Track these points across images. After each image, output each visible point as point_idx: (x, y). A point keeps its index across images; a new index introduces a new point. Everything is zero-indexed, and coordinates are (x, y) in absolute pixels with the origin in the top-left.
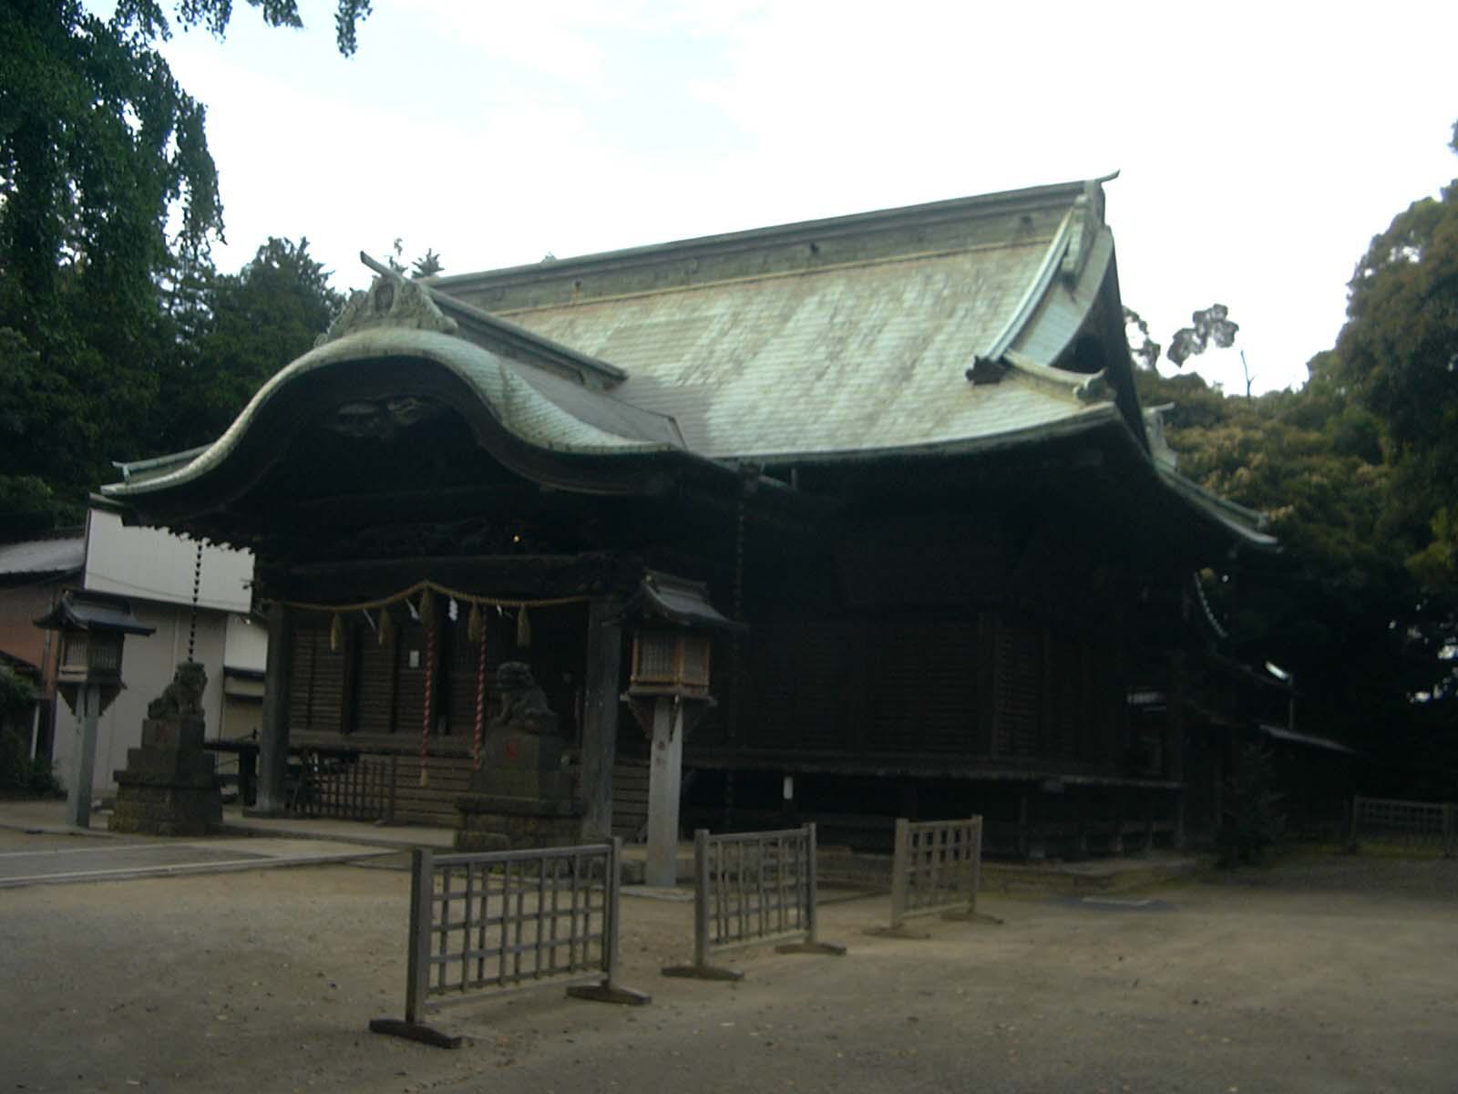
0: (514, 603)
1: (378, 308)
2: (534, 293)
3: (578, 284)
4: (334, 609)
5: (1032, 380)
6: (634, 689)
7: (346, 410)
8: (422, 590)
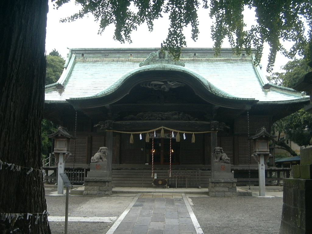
0: (182, 132)
1: (160, 57)
3: (131, 55)
6: (55, 151)
7: (152, 82)
8: (162, 128)
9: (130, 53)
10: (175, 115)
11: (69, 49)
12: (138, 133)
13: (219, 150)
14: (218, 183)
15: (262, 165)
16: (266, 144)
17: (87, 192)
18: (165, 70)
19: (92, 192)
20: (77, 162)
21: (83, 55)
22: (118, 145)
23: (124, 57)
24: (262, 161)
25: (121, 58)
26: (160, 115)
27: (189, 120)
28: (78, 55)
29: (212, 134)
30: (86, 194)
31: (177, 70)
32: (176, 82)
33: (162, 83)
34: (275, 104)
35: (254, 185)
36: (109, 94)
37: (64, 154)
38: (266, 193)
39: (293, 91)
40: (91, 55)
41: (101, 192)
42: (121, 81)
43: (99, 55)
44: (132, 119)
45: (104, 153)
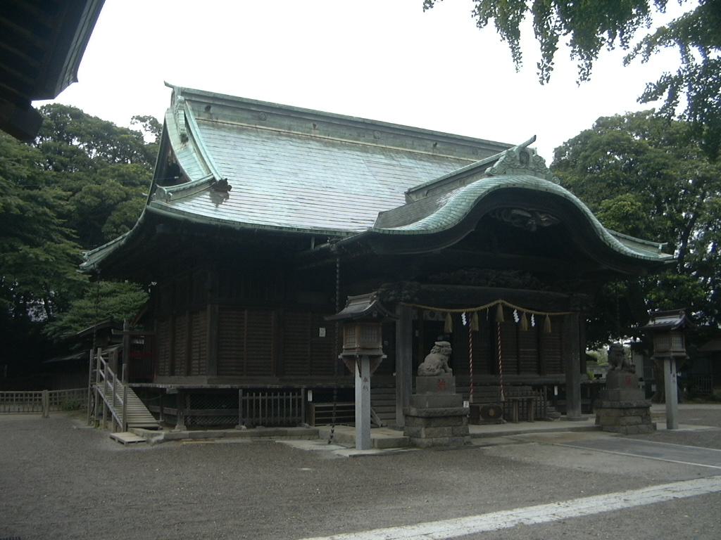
0: (543, 313)
3: (315, 126)
12: (460, 310)
14: (628, 408)
19: (440, 440)
21: (208, 108)
30: (430, 445)
31: (556, 193)
36: (450, 227)
38: (680, 425)
39: (641, 243)
40: (227, 112)
41: (456, 438)
42: (469, 203)
43: (246, 115)
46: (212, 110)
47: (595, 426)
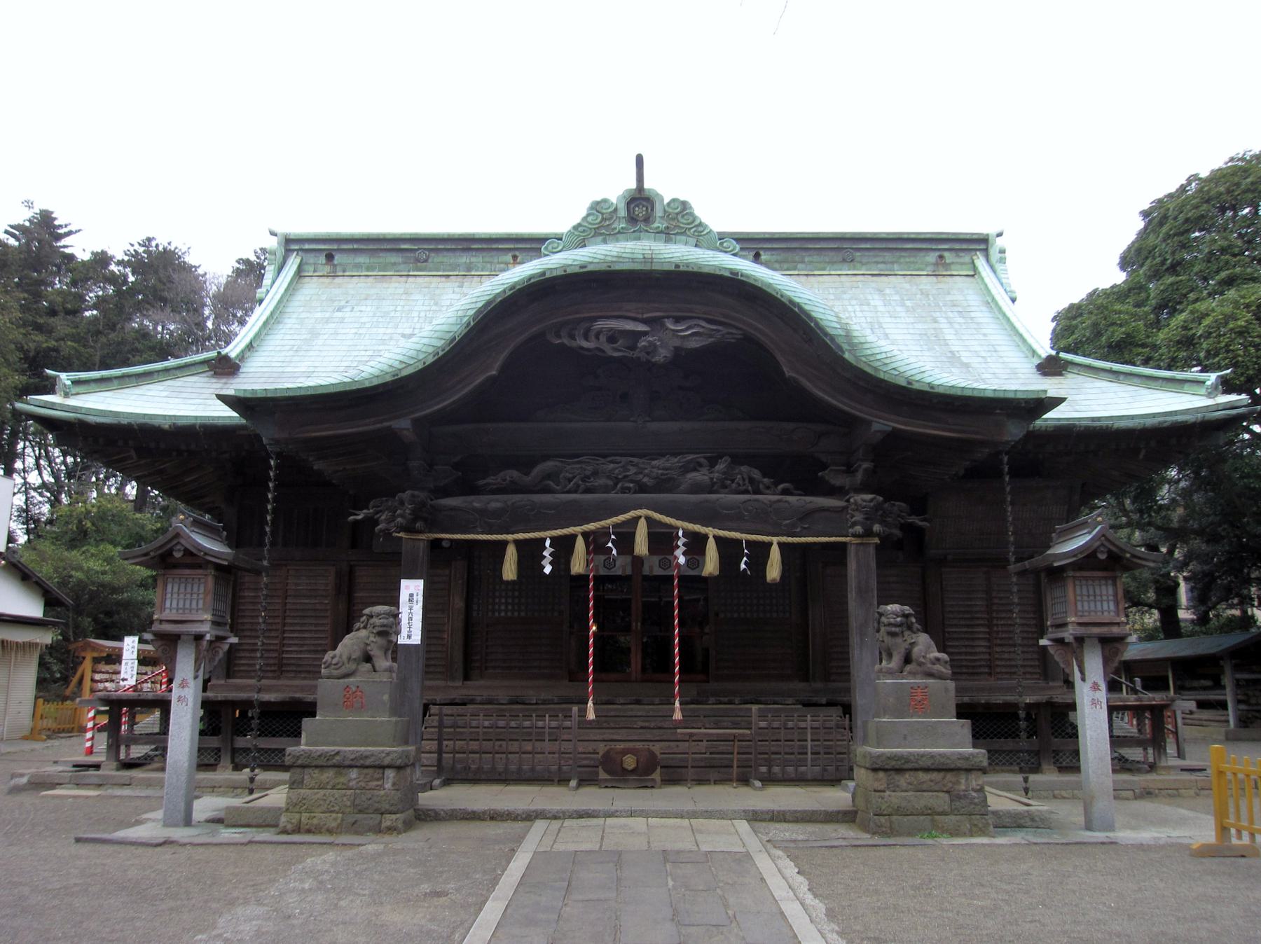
1: (632, 219)
2: (464, 259)
3: (515, 257)
4: (510, 537)
5: (116, 382)
6: (156, 627)
9: (510, 250)
10: (695, 470)
11: (276, 235)
13: (899, 619)
15: (1095, 687)
16: (1111, 591)
17: (297, 816)
18: (656, 267)
20: (288, 671)
22: (458, 603)
23: (489, 265)
24: (1093, 669)
25: (476, 271)
26: (633, 470)
27: (755, 493)
28: (311, 258)
29: (852, 551)
30: (289, 827)
32: (704, 324)
33: (642, 328)
34: (1101, 427)
35: (1017, 768)
37: (198, 637)
40: (361, 259)
44: (515, 488)
45: (380, 634)
46: (338, 259)
47: (851, 809)
